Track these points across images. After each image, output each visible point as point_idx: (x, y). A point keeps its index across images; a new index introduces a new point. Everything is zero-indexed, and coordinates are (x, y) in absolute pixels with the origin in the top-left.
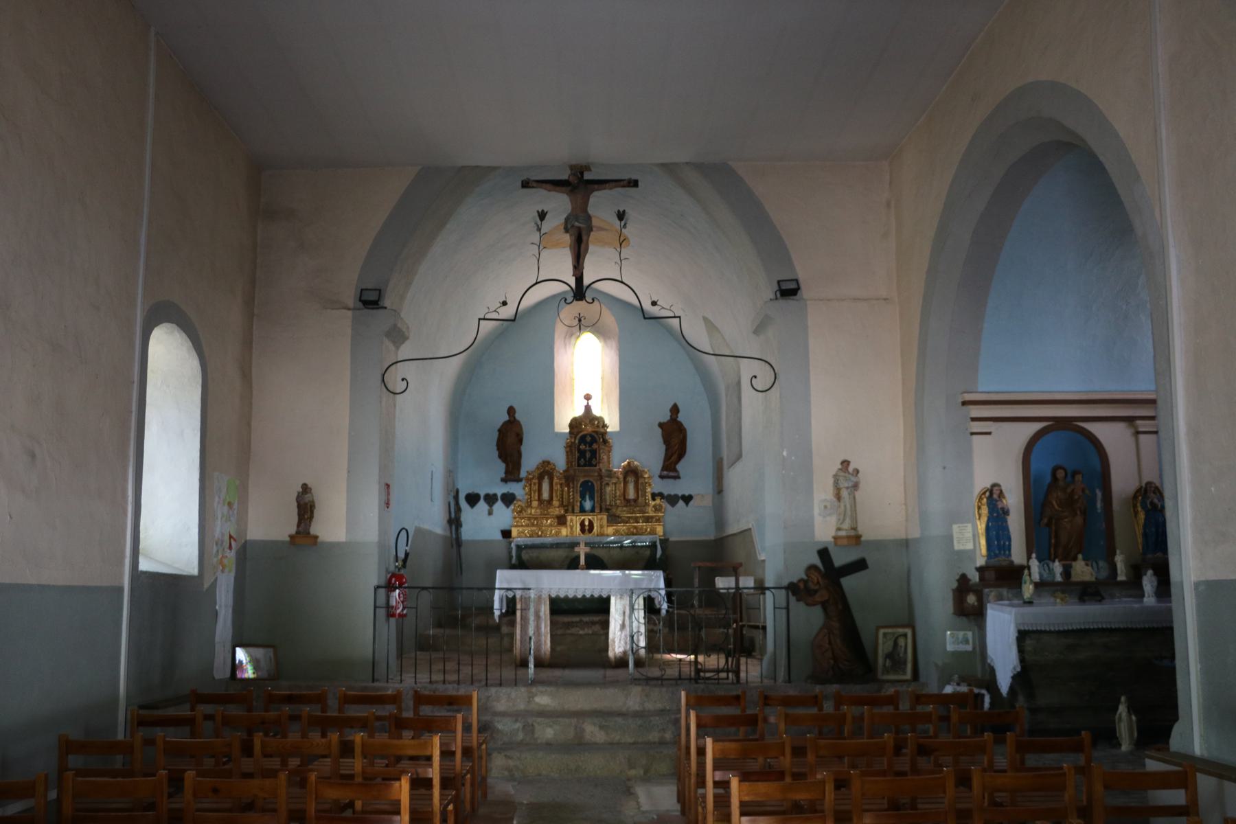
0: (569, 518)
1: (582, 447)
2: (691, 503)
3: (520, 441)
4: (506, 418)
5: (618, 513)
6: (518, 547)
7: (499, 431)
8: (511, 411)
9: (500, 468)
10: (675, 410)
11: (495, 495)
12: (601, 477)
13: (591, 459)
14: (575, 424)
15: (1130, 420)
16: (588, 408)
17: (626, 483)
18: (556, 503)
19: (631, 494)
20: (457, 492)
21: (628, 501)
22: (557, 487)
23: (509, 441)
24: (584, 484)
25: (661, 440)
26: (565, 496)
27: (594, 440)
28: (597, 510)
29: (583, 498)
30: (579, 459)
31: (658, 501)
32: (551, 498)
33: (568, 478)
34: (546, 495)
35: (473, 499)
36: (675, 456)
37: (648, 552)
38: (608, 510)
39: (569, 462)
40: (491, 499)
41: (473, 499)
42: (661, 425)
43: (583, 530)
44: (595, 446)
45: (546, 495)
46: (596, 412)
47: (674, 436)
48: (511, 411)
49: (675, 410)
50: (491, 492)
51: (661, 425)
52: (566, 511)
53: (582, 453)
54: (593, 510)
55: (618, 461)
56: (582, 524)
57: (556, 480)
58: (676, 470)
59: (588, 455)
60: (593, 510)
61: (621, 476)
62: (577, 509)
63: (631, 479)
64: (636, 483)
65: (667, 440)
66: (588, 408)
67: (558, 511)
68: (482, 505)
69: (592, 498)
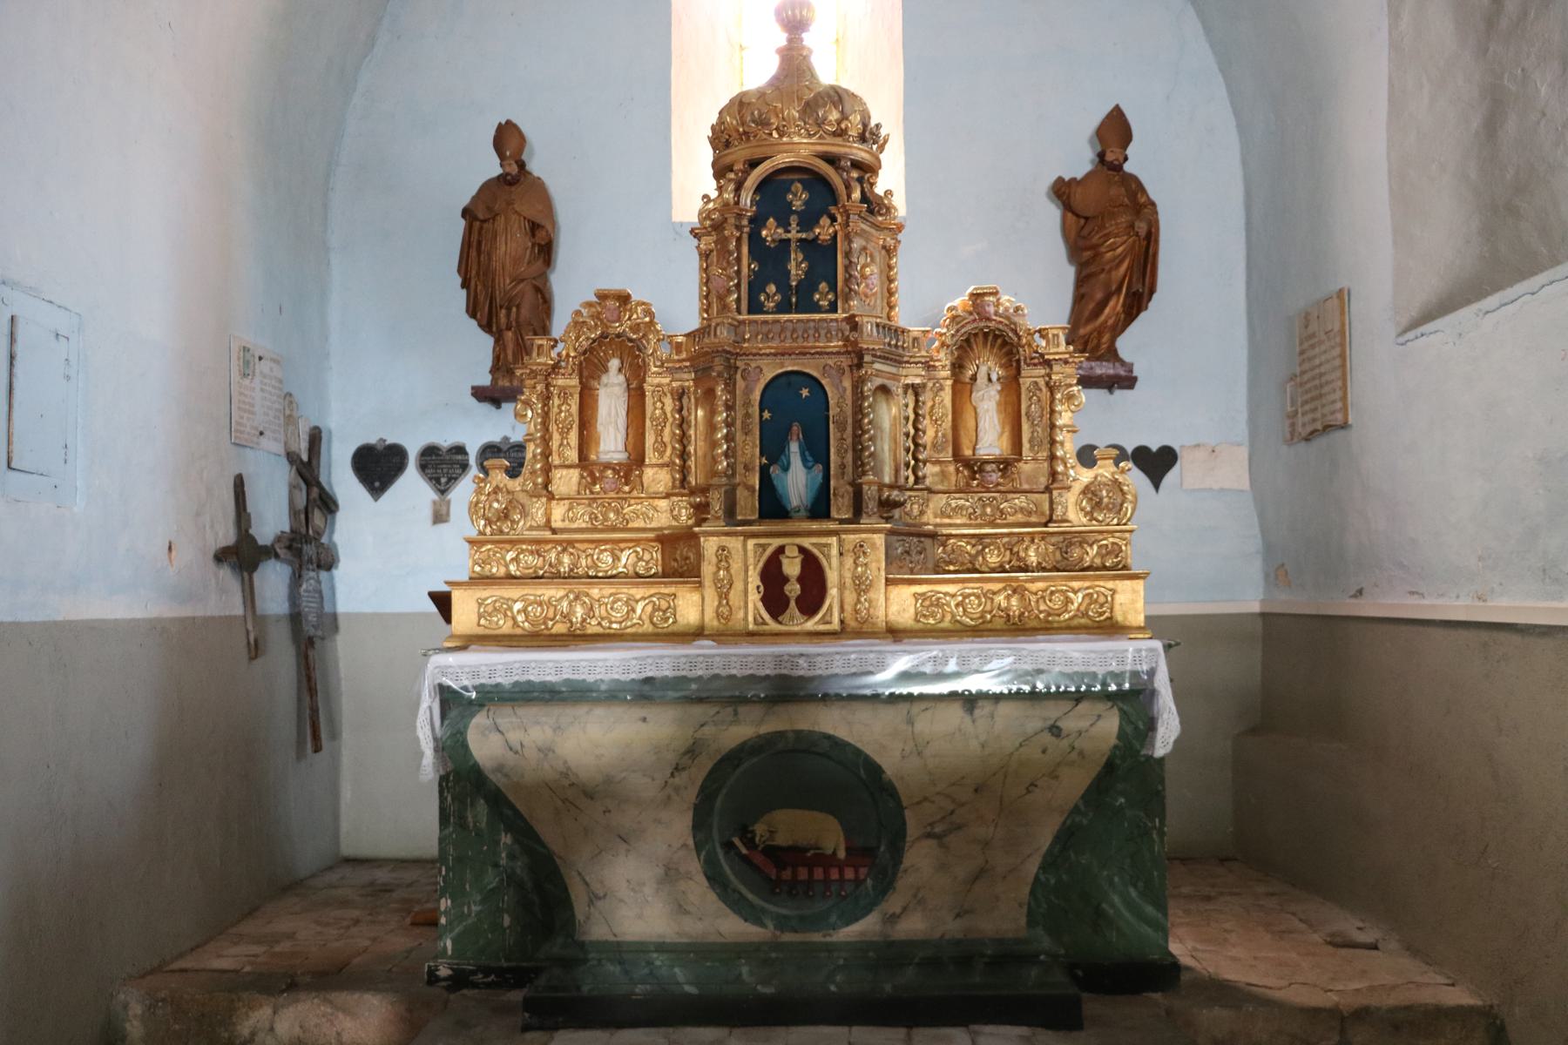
0: (710, 545)
1: (770, 232)
2: (1171, 478)
3: (545, 251)
4: (492, 167)
5: (930, 520)
6: (448, 698)
7: (466, 213)
8: (507, 138)
9: (475, 352)
10: (1115, 131)
11: (460, 450)
12: (857, 357)
13: (808, 286)
14: (738, 134)
15: (554, 531)
16: (794, 63)
17: (962, 387)
18: (657, 477)
19: (990, 440)
20: (315, 438)
21: (973, 467)
22: (660, 407)
23: (505, 247)
24: (782, 390)
25: (1059, 249)
26: (697, 446)
27: (823, 194)
28: (840, 508)
29: (773, 450)
30: (756, 287)
31: (1105, 470)
32: (637, 459)
33: (709, 362)
34: (611, 443)
35: (378, 466)
36: (1116, 305)
37: (1109, 725)
38: (887, 506)
39: (711, 297)
40: (442, 465)
41: (378, 466)
42: (1062, 191)
43: (774, 601)
44: (824, 230)
45: (611, 443)
46: (827, 72)
47: (1110, 232)
48: (507, 138)
49: (1115, 131)
50: (445, 440)
51: (1062, 191)
52: (701, 512)
53: (770, 259)
54: (820, 508)
55: (922, 289)
56: (772, 575)
57: (655, 379)
58: (1112, 355)
59: (796, 267)
60: (820, 508)
61: (944, 359)
62: (748, 504)
63: (987, 367)
64: (1011, 384)
65: (1082, 241)
66: (794, 63)
67: (665, 513)
68: (412, 485)
69: (817, 452)
